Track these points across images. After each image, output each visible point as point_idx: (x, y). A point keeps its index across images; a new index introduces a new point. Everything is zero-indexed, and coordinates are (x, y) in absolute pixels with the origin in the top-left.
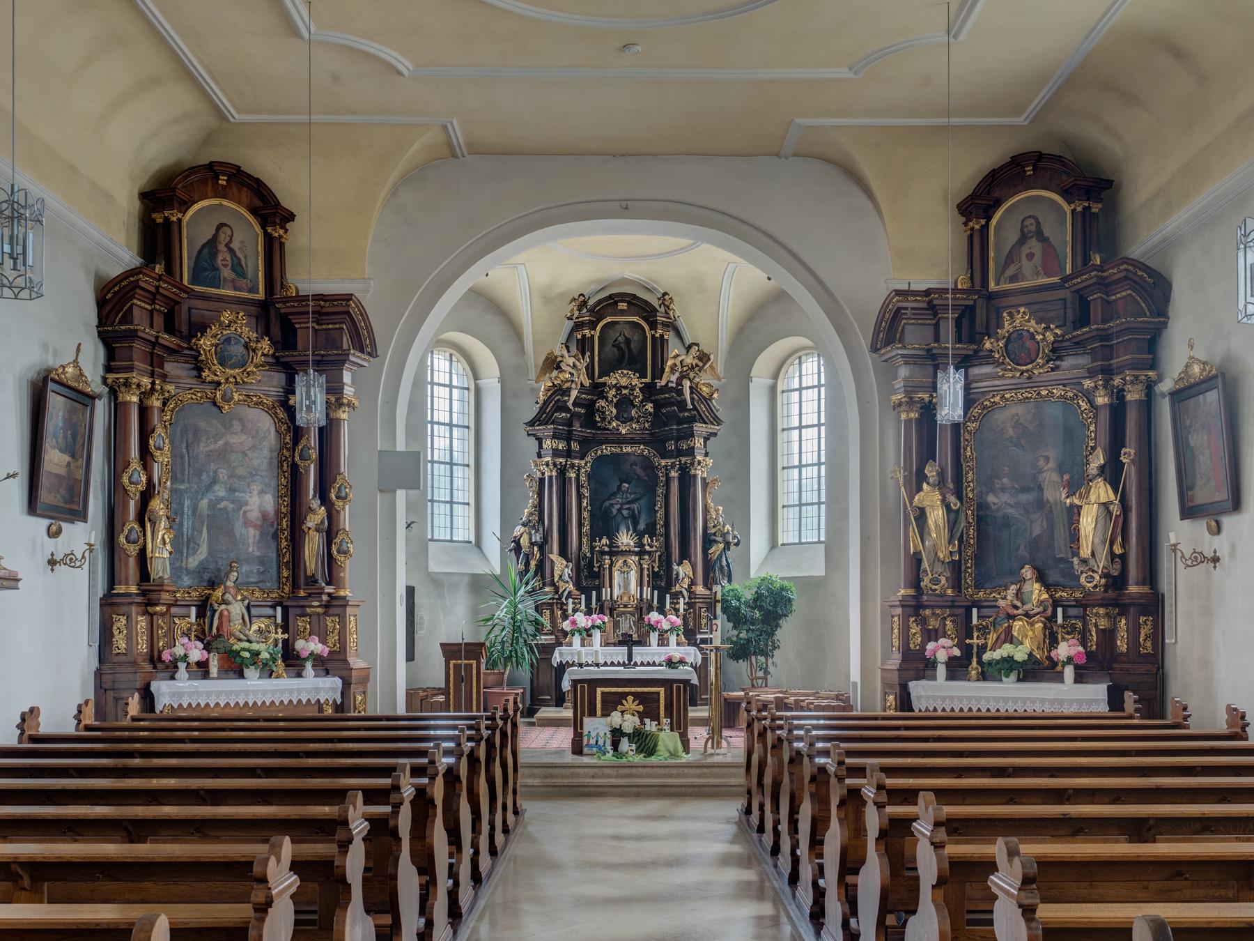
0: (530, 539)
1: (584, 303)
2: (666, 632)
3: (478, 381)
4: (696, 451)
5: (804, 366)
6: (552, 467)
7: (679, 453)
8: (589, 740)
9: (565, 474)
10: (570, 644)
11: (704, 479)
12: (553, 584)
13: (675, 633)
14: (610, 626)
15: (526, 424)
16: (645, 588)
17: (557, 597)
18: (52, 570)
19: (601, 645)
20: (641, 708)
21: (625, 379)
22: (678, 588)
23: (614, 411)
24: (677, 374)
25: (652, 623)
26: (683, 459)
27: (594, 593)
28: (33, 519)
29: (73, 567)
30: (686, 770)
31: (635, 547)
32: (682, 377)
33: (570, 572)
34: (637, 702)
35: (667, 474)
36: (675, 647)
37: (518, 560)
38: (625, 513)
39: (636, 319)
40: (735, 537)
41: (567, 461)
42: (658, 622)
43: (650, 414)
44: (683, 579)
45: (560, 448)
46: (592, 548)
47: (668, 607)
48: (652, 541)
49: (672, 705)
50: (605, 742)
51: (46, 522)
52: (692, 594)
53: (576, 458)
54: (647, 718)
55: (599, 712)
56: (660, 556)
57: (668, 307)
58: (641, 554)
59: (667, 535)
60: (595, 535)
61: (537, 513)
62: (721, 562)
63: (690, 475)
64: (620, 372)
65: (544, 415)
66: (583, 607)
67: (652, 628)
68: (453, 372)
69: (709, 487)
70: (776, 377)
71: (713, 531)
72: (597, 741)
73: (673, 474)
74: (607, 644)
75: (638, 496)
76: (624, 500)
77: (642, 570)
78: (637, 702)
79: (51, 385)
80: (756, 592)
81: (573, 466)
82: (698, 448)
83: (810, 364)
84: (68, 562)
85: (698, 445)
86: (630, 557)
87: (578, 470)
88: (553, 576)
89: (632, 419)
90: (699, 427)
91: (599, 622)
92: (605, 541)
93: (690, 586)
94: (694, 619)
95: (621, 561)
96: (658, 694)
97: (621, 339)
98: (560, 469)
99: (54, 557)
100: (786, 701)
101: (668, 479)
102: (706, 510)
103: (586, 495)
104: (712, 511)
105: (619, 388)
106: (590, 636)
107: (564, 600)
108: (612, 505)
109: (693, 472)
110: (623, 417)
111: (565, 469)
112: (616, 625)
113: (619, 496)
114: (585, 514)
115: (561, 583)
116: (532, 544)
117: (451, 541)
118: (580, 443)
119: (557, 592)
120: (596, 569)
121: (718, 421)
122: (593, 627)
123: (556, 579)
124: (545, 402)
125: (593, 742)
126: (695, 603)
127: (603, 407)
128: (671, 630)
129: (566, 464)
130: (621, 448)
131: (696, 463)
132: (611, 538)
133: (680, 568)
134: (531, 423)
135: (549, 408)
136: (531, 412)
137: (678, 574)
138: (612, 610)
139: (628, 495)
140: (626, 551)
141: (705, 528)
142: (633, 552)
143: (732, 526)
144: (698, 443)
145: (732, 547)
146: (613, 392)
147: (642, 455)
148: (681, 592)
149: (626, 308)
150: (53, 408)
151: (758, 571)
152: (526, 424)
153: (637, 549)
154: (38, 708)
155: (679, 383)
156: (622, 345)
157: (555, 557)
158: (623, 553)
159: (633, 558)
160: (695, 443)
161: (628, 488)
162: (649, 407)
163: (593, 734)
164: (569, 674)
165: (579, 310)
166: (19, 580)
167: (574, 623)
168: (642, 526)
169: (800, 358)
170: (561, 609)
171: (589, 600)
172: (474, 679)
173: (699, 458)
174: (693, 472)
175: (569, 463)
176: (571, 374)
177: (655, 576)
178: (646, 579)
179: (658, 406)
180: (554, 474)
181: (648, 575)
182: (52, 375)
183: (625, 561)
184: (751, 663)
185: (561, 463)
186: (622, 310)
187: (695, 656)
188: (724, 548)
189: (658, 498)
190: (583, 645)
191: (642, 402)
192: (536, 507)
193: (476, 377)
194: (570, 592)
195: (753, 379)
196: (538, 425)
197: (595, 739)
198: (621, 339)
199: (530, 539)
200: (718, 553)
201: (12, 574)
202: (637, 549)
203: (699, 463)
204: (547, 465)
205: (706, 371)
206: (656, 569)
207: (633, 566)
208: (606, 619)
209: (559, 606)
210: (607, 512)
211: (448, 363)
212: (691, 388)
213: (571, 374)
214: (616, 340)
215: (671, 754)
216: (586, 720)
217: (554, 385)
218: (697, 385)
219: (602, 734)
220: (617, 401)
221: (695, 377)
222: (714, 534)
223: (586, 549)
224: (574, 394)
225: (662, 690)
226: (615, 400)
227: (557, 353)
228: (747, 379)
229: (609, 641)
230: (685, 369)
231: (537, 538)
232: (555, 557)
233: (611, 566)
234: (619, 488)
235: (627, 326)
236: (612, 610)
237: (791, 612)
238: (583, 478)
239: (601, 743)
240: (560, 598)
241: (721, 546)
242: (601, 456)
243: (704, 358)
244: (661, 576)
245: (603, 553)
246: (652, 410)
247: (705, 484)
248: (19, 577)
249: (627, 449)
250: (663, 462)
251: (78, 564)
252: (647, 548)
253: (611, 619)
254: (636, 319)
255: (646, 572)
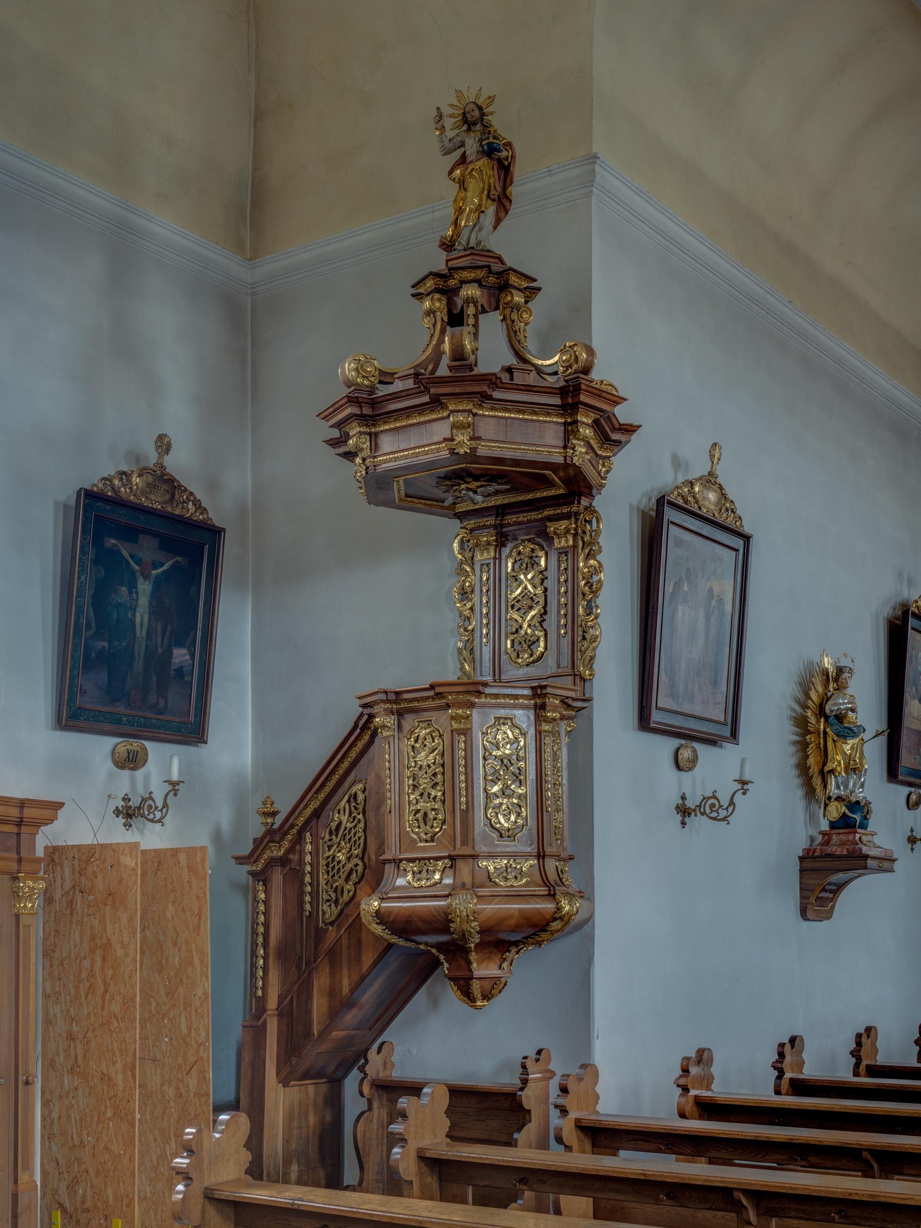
18: (912, 850)
28: (893, 787)
29: (715, 819)
51: (906, 790)
79: (670, 514)
84: (708, 810)
99: (914, 834)
150: (913, 649)
154: (875, 1028)
166: (894, 861)
182: (912, 609)
201: (888, 854)
248: (895, 856)
251: (723, 813)
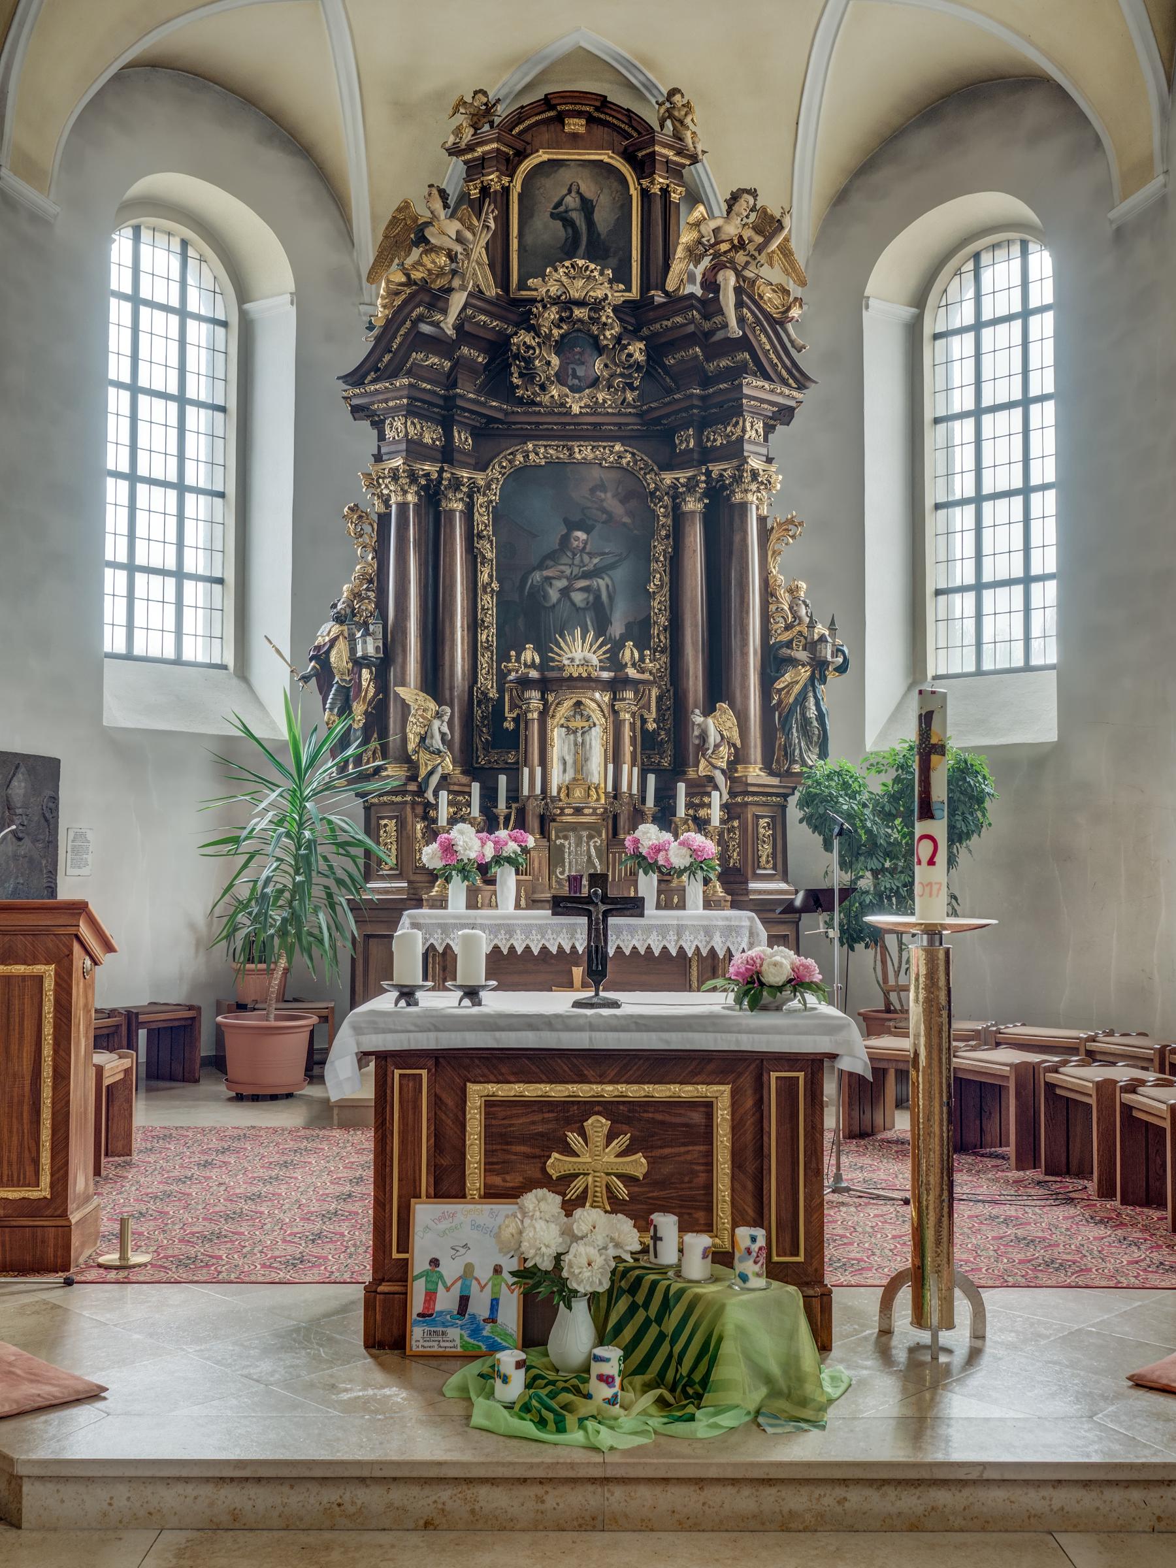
0: (353, 650)
1: (489, 109)
2: (680, 872)
3: (247, 306)
4: (747, 447)
5: (986, 276)
6: (403, 481)
7: (706, 455)
8: (431, 1296)
9: (438, 503)
10: (441, 903)
11: (762, 520)
12: (406, 759)
13: (700, 875)
14: (539, 859)
15: (346, 378)
16: (626, 768)
17: (412, 787)
19: (518, 906)
20: (638, 1165)
21: (580, 283)
22: (703, 769)
23: (555, 361)
24: (706, 262)
25: (644, 851)
26: (716, 469)
27: (503, 779)
30: (855, 1498)
31: (602, 669)
32: (716, 268)
33: (445, 729)
34: (623, 1140)
35: (676, 508)
36: (701, 911)
37: (324, 704)
38: (578, 598)
39: (605, 156)
40: (838, 651)
41: (441, 471)
42: (658, 849)
43: (638, 367)
44: (717, 746)
45: (427, 440)
46: (502, 676)
47: (681, 811)
48: (642, 659)
49: (760, 1152)
50: (494, 1304)
52: (738, 787)
53: (465, 465)
54: (665, 1210)
55: (475, 1178)
56: (659, 699)
57: (681, 122)
58: (616, 686)
59: (675, 651)
60: (508, 645)
61: (372, 595)
62: (804, 709)
63: (733, 506)
64: (567, 263)
65: (387, 358)
66: (475, 811)
67: (644, 862)
68: (190, 281)
69: (774, 536)
70: (920, 300)
71: (786, 637)
72: (464, 1301)
73: (693, 505)
74: (533, 904)
75: (610, 560)
76: (576, 570)
77: (618, 726)
78: (623, 1140)
80: (897, 780)
81: (456, 484)
82: (750, 441)
83: (1001, 268)
85: (750, 434)
86: (589, 694)
87: (470, 496)
88: (404, 740)
89: (595, 383)
90: (753, 387)
91: (512, 848)
92: (530, 654)
93: (733, 764)
94: (743, 844)
95: (568, 704)
96: (708, 1107)
97: (572, 201)
98: (423, 488)
100: (1052, 1077)
101: (678, 517)
102: (768, 593)
103: (489, 555)
104: (782, 593)
105: (567, 304)
106: (491, 882)
107: (429, 795)
108: (548, 580)
109: (738, 497)
110: (575, 376)
111: (437, 492)
112: (555, 857)
113: (565, 560)
114: (487, 601)
115: (423, 757)
116: (359, 663)
117: (178, 662)
118: (476, 434)
119: (413, 778)
120: (509, 725)
121: (802, 381)
122: (498, 860)
123: (411, 746)
124: (389, 322)
125: (446, 1302)
126: (746, 804)
127: (529, 347)
128: (691, 870)
129: (440, 478)
130: (570, 449)
131: (747, 477)
132: (541, 649)
133: (710, 721)
134: (356, 378)
135: (398, 340)
136: (360, 347)
137: (703, 737)
138: (545, 822)
139: (586, 558)
140: (580, 678)
141: (766, 632)
142: (597, 680)
143: (832, 627)
144: (753, 429)
145: (831, 676)
146: (552, 314)
147: (617, 467)
148: (711, 779)
149: (582, 130)
151: (883, 735)
152: (346, 378)
153: (606, 675)
155: (711, 285)
156: (575, 215)
157: (409, 692)
158: (574, 683)
159: (597, 695)
160: (744, 430)
161: (586, 543)
162: (637, 350)
163: (450, 1270)
164: (357, 1030)
165: (476, 127)
167: (449, 849)
168: (617, 629)
169: (977, 256)
170: (425, 817)
171: (489, 797)
172: (48, 1030)
173: (755, 463)
174: (738, 497)
175: (446, 475)
176: (452, 257)
177: (648, 742)
178: (628, 749)
179: (655, 352)
180: (411, 498)
181: (633, 740)
183: (579, 704)
184: (884, 949)
185: (427, 475)
186: (575, 136)
187: (751, 934)
188: (812, 678)
189: (654, 566)
190: (472, 904)
191: (618, 339)
192: (370, 581)
193: (243, 295)
194: (444, 778)
195: (871, 302)
196: (374, 381)
197: (456, 1291)
198: (572, 201)
199: (353, 650)
200: (797, 689)
202: (606, 675)
203: (755, 475)
204: (395, 477)
205: (770, 257)
206: (651, 726)
207: (597, 716)
208: (531, 841)
209: (419, 810)
210: (535, 599)
211: (176, 263)
212: (738, 291)
213: (452, 257)
214: (559, 204)
215: (775, 1393)
216: (425, 1213)
217: (410, 282)
218: (753, 283)
219: (484, 1273)
220: (562, 336)
221: (747, 263)
222: (789, 644)
223: (487, 683)
224: (458, 301)
225: (721, 1094)
226: (556, 332)
227: (424, 214)
228: (859, 302)
229: (537, 896)
230: (724, 247)
231: (369, 647)
232: (409, 692)
233: (544, 714)
234: (565, 540)
235: (586, 172)
236: (545, 822)
237: (979, 827)
238: (482, 518)
239: (479, 1307)
240: (421, 792)
241: (804, 673)
242: (524, 468)
243: (769, 225)
244: (662, 743)
245: (525, 683)
246: (639, 357)
247: (765, 534)
249: (584, 452)
250: (668, 478)
252: (632, 672)
253: (545, 843)
254: (605, 156)
255: (627, 733)
